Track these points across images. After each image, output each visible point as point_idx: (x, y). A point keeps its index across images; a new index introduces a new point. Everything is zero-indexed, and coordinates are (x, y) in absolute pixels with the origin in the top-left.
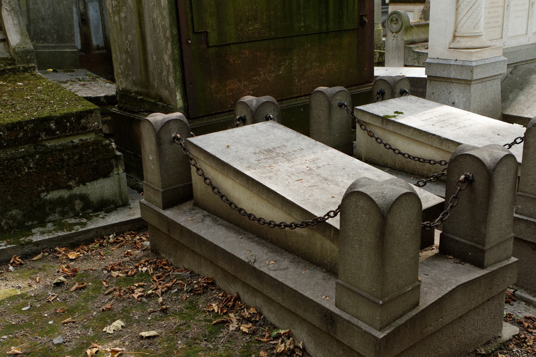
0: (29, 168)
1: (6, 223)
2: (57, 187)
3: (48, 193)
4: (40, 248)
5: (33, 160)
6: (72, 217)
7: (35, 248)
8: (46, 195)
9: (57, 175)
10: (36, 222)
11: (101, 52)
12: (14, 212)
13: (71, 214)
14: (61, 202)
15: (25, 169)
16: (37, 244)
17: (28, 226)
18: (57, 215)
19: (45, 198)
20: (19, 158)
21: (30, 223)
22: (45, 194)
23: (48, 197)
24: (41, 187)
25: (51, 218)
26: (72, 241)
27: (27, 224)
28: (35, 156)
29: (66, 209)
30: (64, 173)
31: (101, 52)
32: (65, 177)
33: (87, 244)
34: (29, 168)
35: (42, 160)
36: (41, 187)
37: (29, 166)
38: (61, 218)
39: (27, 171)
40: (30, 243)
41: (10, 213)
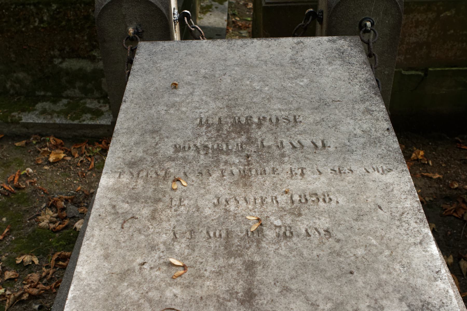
0: (41, 21)
1: (12, 86)
2: (75, 54)
3: (64, 59)
4: (31, 131)
5: (48, 10)
6: (95, 99)
7: (24, 130)
8: (61, 63)
9: (75, 38)
10: (49, 94)
11: (173, 10)
12: (21, 75)
13: (97, 94)
14: (81, 75)
15: (35, 22)
16: (27, 125)
17: (38, 96)
18: (77, 91)
19: (60, 66)
20: (30, 4)
21: (42, 93)
22: (60, 60)
23: (64, 65)
24: (53, 50)
25: (69, 92)
26: (75, 134)
27: (37, 93)
28: (51, 6)
29: (89, 86)
30: (86, 38)
31: (173, 10)
32: (87, 44)
33: (91, 143)
34: (41, 21)
35: (59, 13)
36: (53, 50)
37: (42, 18)
38: (83, 95)
39: (36, 24)
40: (16, 122)
41: (15, 75)
